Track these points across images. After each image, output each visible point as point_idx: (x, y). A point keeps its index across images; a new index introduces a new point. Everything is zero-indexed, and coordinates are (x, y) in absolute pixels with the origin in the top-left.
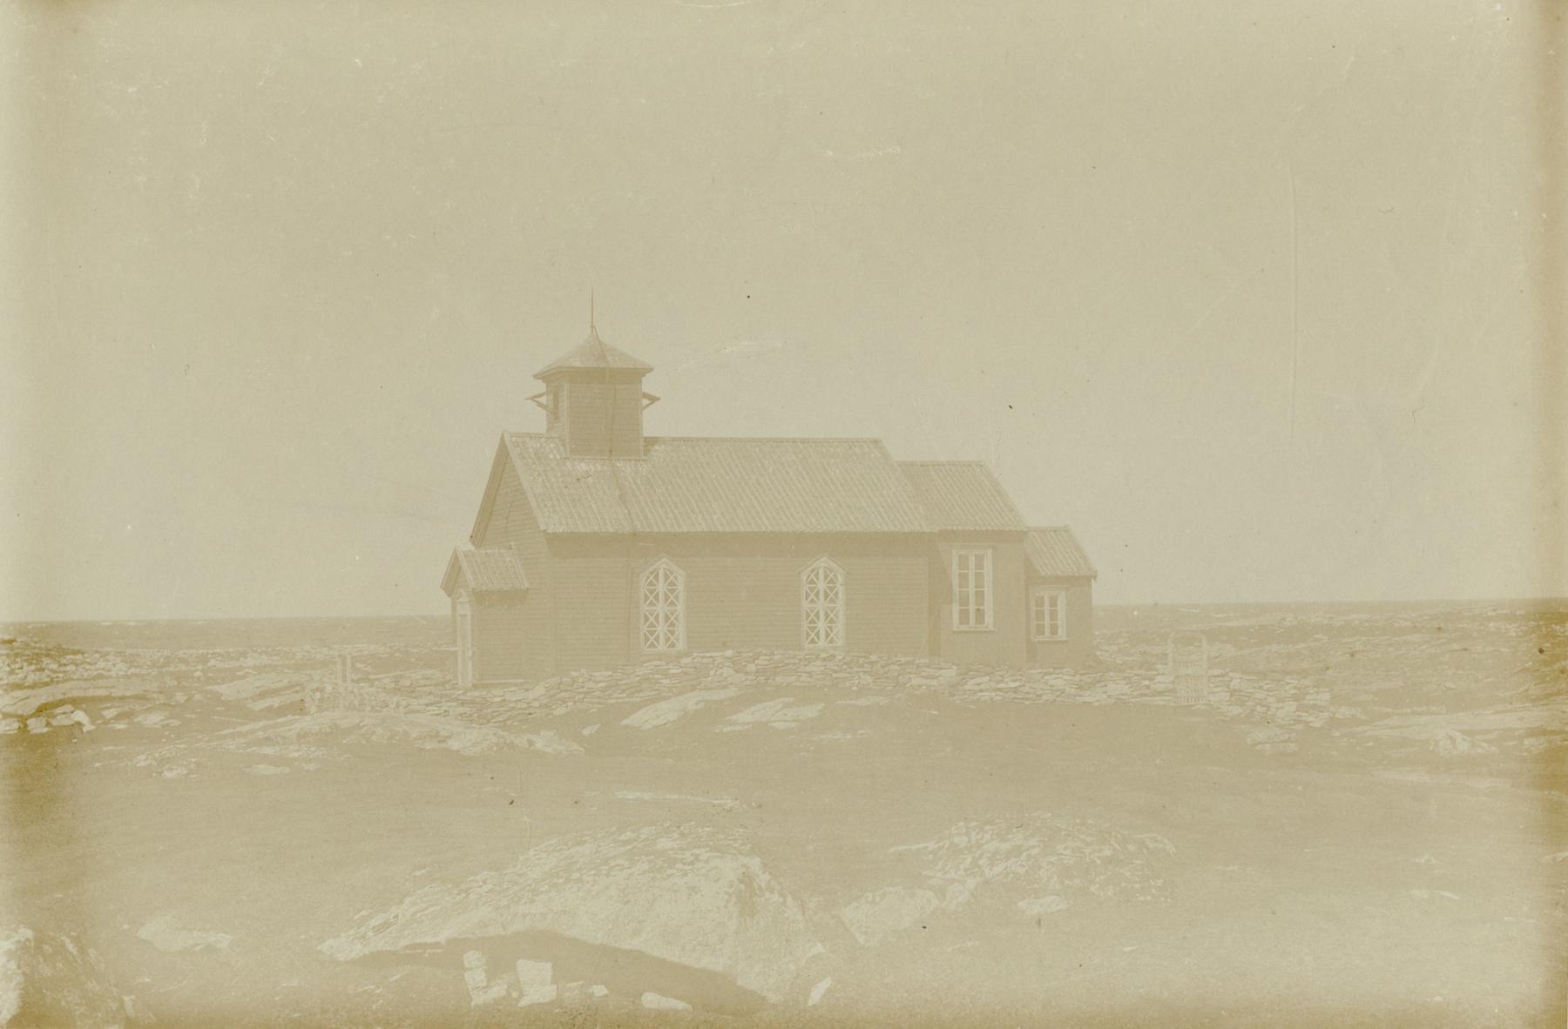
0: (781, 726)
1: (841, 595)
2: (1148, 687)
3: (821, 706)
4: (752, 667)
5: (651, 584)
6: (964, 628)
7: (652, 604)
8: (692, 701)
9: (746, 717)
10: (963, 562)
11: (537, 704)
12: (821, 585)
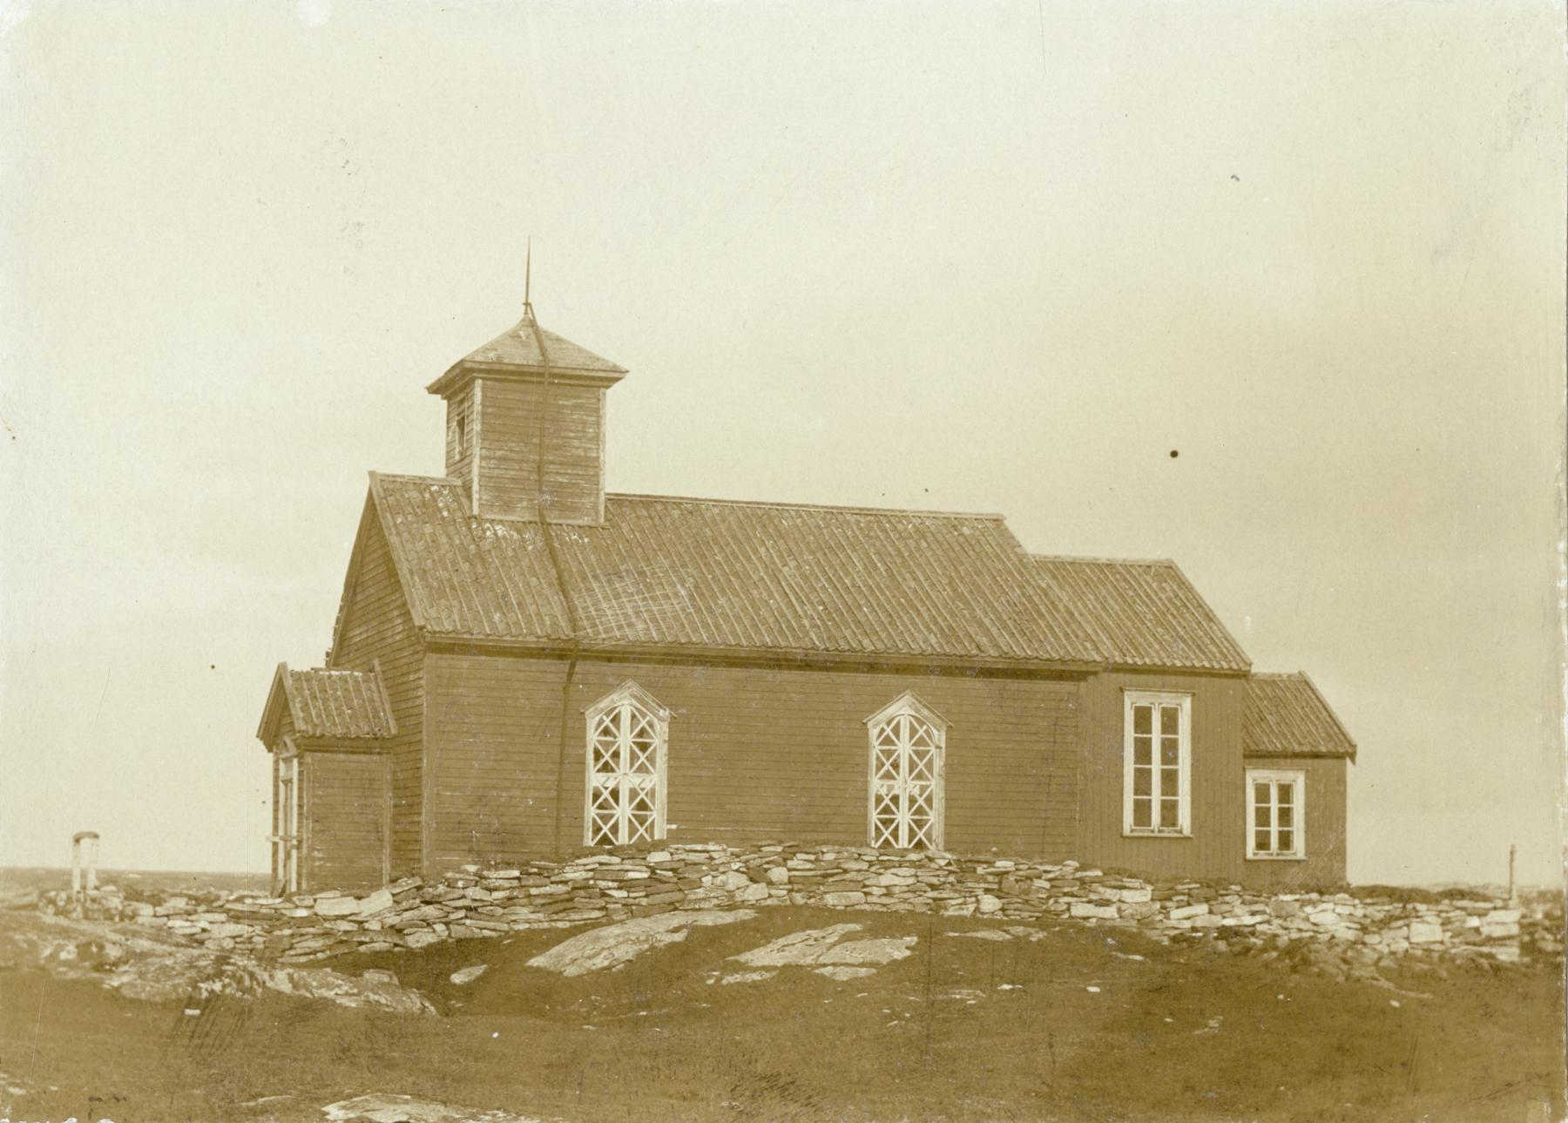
0: (843, 975)
1: (938, 764)
2: (1477, 930)
3: (912, 940)
4: (779, 874)
5: (606, 732)
6: (1142, 832)
7: (888, 776)
8: (663, 929)
9: (768, 956)
10: (1143, 718)
11: (374, 925)
12: (904, 748)
